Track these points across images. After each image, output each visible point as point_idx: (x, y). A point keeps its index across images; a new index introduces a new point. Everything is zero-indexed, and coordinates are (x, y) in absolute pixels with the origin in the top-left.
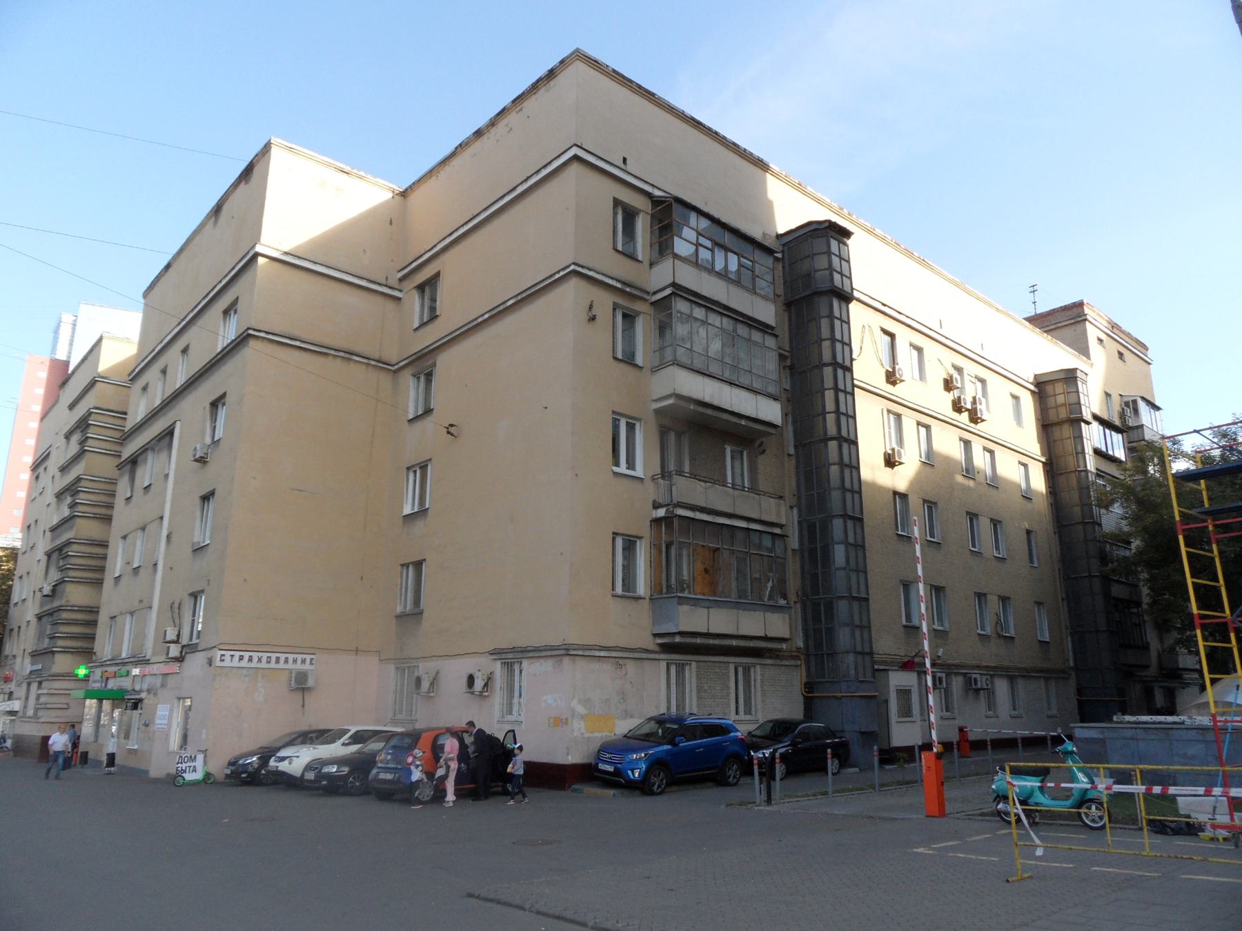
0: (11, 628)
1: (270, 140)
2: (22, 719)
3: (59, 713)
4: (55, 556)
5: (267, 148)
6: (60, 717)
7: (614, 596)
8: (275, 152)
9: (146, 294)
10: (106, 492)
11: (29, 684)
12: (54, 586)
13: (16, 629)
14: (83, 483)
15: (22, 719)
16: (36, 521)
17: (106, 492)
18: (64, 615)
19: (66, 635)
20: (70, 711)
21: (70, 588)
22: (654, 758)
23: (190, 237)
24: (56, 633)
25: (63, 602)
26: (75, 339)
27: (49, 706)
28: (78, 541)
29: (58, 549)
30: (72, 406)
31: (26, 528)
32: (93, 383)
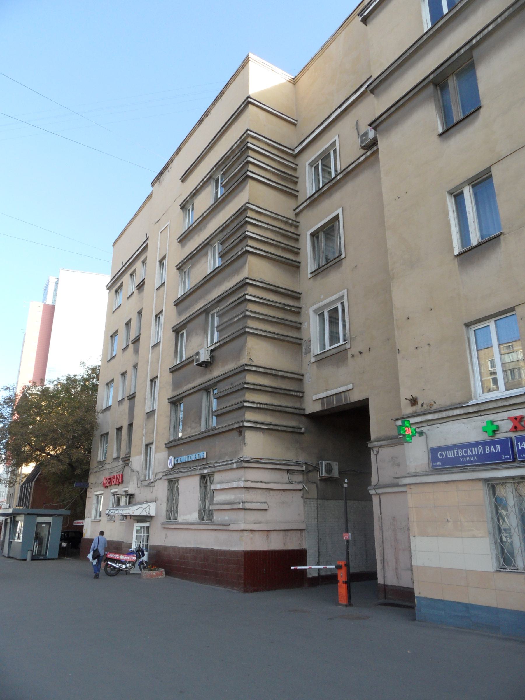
0: (104, 432)
1: (248, 55)
2: (167, 526)
3: (258, 516)
4: (322, 235)
5: (247, 60)
6: (260, 523)
7: (138, 487)
8: (251, 64)
9: (114, 244)
10: (274, 228)
11: (173, 484)
12: (212, 351)
13: (113, 434)
14: (250, 214)
15: (167, 526)
16: (140, 313)
17: (274, 228)
18: (250, 378)
19: (255, 405)
20: (269, 513)
21: (251, 343)
22: (515, 556)
23: (53, 320)
24: (245, 401)
25: (244, 360)
26: (58, 292)
27: (248, 506)
28: (254, 283)
29: (204, 311)
30: (184, 178)
31: (110, 338)
32: (247, 102)
